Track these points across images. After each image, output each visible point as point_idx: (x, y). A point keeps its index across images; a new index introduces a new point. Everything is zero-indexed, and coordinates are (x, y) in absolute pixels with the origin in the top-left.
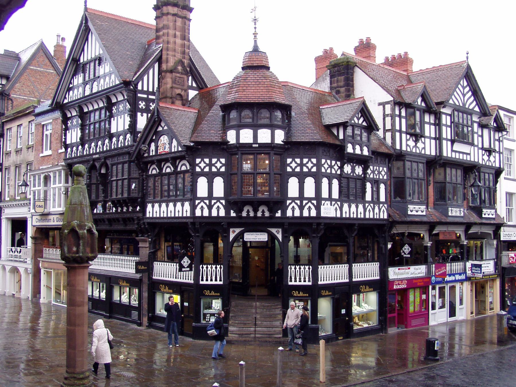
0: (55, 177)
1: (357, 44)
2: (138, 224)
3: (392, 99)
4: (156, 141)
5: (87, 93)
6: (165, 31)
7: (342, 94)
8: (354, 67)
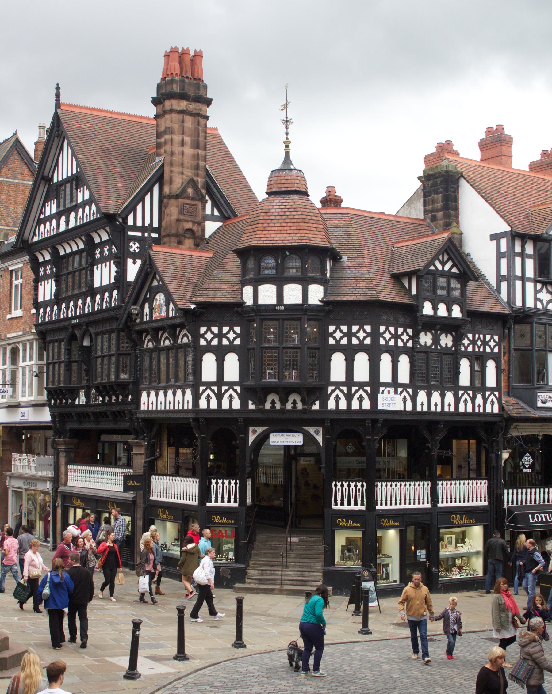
0: (25, 350)
1: (483, 136)
2: (131, 419)
3: (508, 229)
4: (151, 301)
5: (63, 228)
6: (168, 137)
7: (439, 222)
8: (459, 178)
